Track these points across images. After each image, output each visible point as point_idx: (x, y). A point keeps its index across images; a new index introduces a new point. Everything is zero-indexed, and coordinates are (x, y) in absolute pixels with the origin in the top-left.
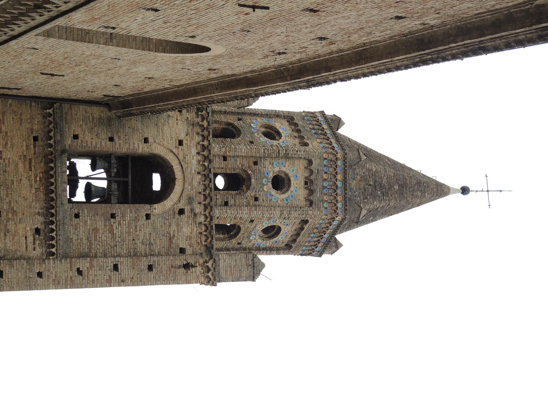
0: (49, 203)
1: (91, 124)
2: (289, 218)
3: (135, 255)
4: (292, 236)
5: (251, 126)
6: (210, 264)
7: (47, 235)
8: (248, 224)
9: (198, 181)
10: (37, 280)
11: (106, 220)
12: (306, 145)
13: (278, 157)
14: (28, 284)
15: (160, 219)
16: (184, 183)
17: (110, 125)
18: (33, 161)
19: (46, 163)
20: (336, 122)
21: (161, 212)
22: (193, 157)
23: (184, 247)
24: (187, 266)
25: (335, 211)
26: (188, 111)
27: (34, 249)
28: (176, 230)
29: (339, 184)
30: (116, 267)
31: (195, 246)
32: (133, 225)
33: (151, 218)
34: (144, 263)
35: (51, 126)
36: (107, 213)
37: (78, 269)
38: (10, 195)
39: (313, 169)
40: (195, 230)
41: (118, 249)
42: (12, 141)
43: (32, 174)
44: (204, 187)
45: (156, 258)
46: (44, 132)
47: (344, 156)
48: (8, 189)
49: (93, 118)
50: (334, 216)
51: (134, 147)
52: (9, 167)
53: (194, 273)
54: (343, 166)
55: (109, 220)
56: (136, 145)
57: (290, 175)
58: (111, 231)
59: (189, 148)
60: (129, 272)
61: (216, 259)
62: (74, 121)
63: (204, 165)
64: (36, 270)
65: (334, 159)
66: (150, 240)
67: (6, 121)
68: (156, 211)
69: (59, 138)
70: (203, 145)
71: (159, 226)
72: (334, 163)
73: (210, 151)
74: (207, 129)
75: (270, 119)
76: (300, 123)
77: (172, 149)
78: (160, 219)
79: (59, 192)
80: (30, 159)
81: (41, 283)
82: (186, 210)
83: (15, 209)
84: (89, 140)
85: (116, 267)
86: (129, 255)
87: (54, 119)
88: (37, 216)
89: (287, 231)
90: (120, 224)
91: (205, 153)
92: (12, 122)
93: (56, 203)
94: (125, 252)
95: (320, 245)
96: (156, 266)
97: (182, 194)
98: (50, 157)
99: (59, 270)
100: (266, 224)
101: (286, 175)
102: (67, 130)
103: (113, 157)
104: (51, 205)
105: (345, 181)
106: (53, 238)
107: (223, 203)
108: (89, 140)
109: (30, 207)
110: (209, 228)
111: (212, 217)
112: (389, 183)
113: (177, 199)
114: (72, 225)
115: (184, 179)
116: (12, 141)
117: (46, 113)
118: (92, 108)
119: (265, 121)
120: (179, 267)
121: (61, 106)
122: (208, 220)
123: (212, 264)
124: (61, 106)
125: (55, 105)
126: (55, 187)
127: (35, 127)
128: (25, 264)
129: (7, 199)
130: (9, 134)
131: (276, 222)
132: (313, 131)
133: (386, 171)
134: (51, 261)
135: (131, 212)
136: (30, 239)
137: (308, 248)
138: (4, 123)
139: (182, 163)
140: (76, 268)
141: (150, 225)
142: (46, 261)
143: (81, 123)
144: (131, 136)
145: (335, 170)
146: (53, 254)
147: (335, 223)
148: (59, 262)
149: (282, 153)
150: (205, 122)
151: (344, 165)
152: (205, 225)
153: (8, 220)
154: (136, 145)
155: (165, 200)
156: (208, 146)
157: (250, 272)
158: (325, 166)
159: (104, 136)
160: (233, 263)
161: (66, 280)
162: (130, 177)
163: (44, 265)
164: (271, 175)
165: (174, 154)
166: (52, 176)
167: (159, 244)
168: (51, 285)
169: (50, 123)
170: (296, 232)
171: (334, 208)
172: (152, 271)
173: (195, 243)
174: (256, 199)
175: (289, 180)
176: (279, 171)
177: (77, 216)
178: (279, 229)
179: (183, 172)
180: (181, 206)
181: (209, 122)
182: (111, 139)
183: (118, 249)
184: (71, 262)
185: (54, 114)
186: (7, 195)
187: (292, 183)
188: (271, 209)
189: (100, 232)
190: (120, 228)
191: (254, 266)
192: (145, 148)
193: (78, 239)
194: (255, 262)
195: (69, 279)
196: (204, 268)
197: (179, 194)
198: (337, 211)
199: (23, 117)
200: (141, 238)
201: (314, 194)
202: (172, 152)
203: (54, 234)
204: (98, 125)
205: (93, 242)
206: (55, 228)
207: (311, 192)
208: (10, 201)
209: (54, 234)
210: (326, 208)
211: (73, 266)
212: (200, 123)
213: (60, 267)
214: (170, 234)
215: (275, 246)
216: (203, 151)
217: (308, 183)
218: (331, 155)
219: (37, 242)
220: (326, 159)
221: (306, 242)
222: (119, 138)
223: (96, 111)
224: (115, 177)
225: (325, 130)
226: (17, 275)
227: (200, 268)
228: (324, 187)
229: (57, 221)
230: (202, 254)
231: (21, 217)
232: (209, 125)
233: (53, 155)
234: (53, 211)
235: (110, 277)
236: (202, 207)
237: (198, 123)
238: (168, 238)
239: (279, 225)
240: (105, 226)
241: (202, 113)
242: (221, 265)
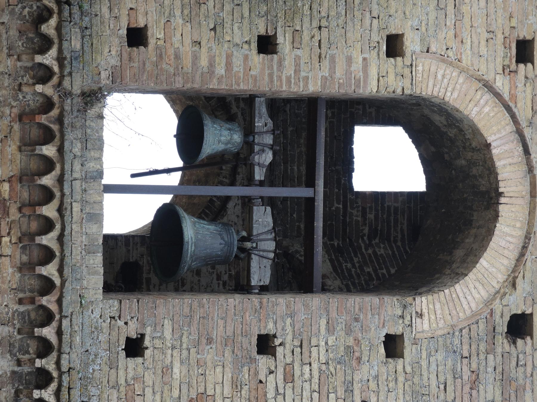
0: (32, 301)
11: (238, 365)
19: (28, 145)
32: (338, 381)
36: (245, 334)
46: (22, 17)
55: (252, 360)
56: (357, 66)
68: (423, 326)
69: (76, 44)
77: (489, 77)
78: (440, 356)
84: (187, 49)
90: (289, 378)
93: (59, 302)
97: (522, 255)
102: (105, 10)
103: (261, 111)
104: (42, 307)
113: (501, 278)
114: (116, 386)
126: (61, 239)
135: (330, 330)
141: (401, 379)
154: (357, 66)
162: (320, 183)
165: (497, 95)
166: (47, 196)
177: (134, 347)
182: (266, 45)
190: (289, 392)
192: (391, 77)
197: (513, 255)
202: (489, 87)
222: (295, 43)
224: (271, 180)
233: (55, 112)
240: (237, 385)
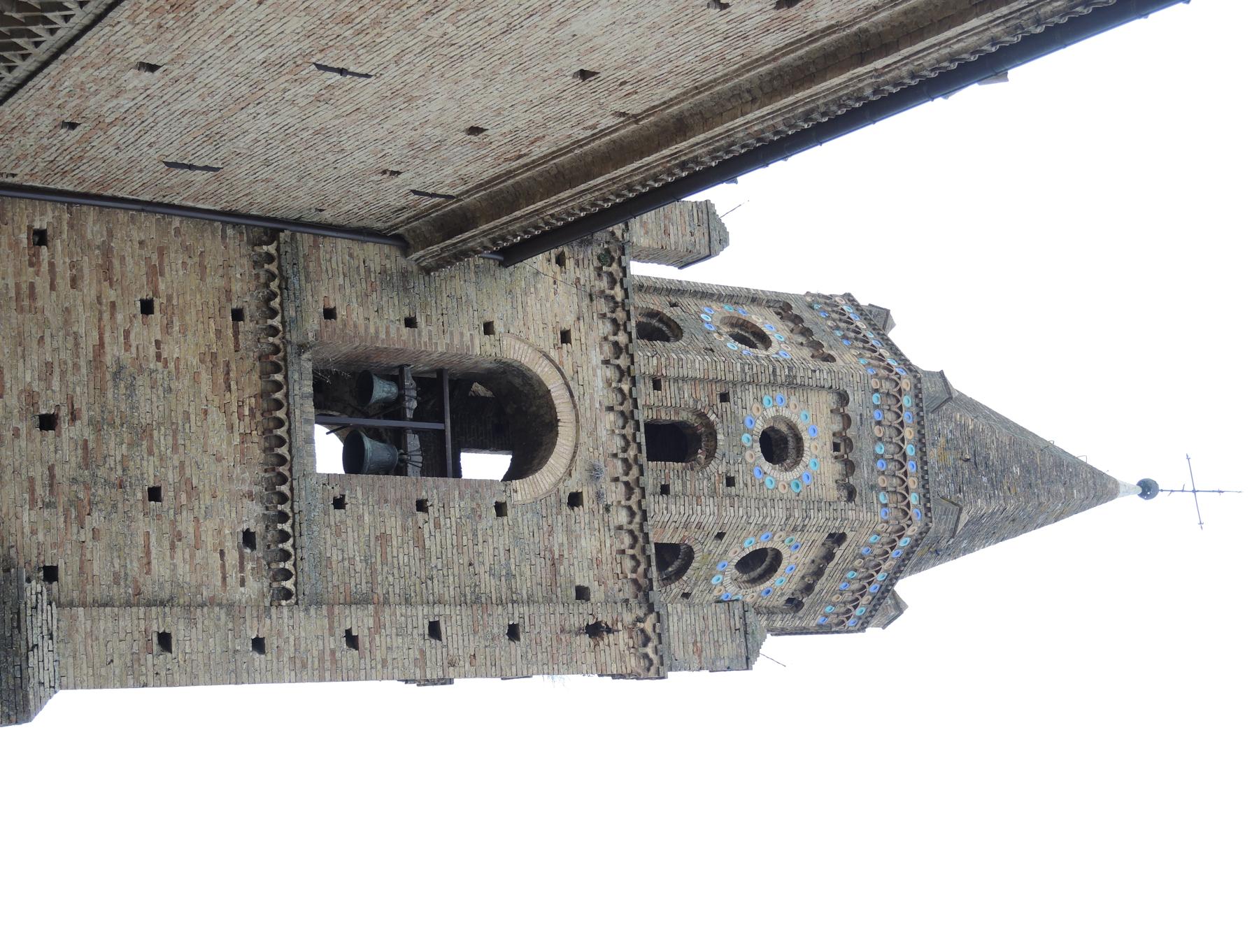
0: (273, 470)
1: (364, 285)
2: (804, 526)
3: (477, 600)
4: (803, 577)
5: (702, 321)
6: (648, 626)
7: (273, 547)
8: (711, 544)
9: (608, 427)
10: (255, 657)
11: (405, 517)
12: (829, 359)
13: (772, 384)
14: (232, 667)
15: (529, 515)
16: (577, 432)
17: (406, 290)
18: (233, 366)
19: (264, 374)
20: (879, 319)
21: (529, 499)
22: (594, 370)
23: (586, 584)
24: (595, 630)
25: (906, 514)
26: (577, 263)
27: (243, 583)
28: (565, 542)
29: (910, 450)
30: (434, 630)
31: (610, 583)
32: (468, 529)
33: (509, 513)
34: (499, 621)
35: (274, 285)
37: (348, 632)
38: (181, 449)
39: (850, 414)
40: (608, 545)
41: (437, 587)
42: (182, 318)
43: (233, 398)
44: (623, 444)
45: (526, 608)
47: (916, 386)
48: (175, 433)
49: (368, 270)
50: (904, 523)
51: (462, 341)
52: (178, 379)
53: (613, 647)
54: (914, 409)
55: (414, 514)
56: (467, 338)
57: (800, 427)
58: (419, 542)
59: (585, 350)
60: (466, 642)
61: (662, 612)
62: (324, 276)
63: (621, 390)
64: (249, 632)
65: (894, 391)
66: (508, 564)
67: (167, 269)
68: (518, 497)
69: (293, 313)
70: (616, 344)
71: (526, 532)
72: (894, 401)
73: (632, 356)
74: (623, 304)
75: (739, 308)
76: (806, 315)
77: (546, 350)
78: (529, 515)
79: (299, 440)
80: (227, 364)
81: (263, 666)
82: (585, 495)
83: (195, 482)
84: (361, 322)
85: (434, 630)
86: (462, 602)
87: (280, 267)
88: (246, 501)
89: (795, 564)
90: (437, 525)
91: (623, 361)
92: (181, 273)
94: (452, 593)
95: (864, 601)
96: (527, 629)
98: (274, 358)
99: (303, 634)
100: (750, 546)
101: (792, 427)
105: (921, 442)
106: (286, 556)
107: (659, 490)
108: (361, 322)
109: (230, 478)
110: (641, 540)
111: (644, 512)
112: (1003, 460)
113: (563, 470)
114: (329, 526)
115: (577, 421)
116: (182, 318)
117: (260, 255)
118: (365, 246)
119: (728, 309)
120: (578, 633)
121: (293, 237)
122: (637, 519)
123: (654, 626)
124: (293, 237)
125: (282, 235)
126: (289, 431)
127: (236, 287)
128: (223, 616)
129: (176, 457)
130: (175, 302)
131: (772, 539)
132: (839, 334)
133: (994, 432)
134: (285, 610)
135: (461, 497)
136: (232, 557)
137: (837, 610)
138: (162, 274)
139: (571, 384)
140: (343, 629)
142: (273, 610)
143: (341, 281)
144: (454, 317)
145: (899, 416)
146: (287, 594)
147: (903, 543)
148: (302, 614)
149: (782, 374)
150: (618, 288)
151: (917, 405)
152: (631, 532)
153: (179, 510)
154: (467, 338)
155: (536, 471)
156: (627, 346)
157: (739, 646)
158: (877, 407)
159: (394, 313)
160: (700, 625)
161: (321, 660)
163: (268, 621)
164: (760, 427)
165: (552, 361)
166: (279, 405)
167: (530, 577)
168: (286, 671)
169: (272, 276)
170: (813, 568)
171: (903, 505)
172: (519, 639)
173: (610, 575)
174: (730, 482)
175: (799, 440)
176: (775, 418)
178: (777, 557)
179: (575, 406)
180: (572, 486)
181: (626, 290)
182: (410, 323)
183: (437, 587)
184: (331, 615)
185: (279, 255)
186: (175, 448)
187: (806, 445)
188: (766, 506)
189: (394, 543)
190: (438, 535)
191: (746, 633)
192: (488, 346)
193: (343, 559)
194: (748, 621)
195: (327, 657)
196: (634, 634)
197: (570, 457)
198: (910, 513)
199: (208, 260)
200: (488, 559)
201: (857, 471)
202: (547, 356)
203: (288, 546)
204: (379, 289)
205: (379, 568)
206: (290, 530)
207: (850, 467)
208: (182, 464)
209: (288, 546)
210: (886, 505)
211: (336, 624)
212: (608, 292)
213: (298, 627)
214: (552, 552)
215: (764, 603)
216: (618, 358)
217: (842, 445)
218: (888, 383)
219: (249, 566)
220: (877, 391)
221: (834, 593)
223: (375, 255)
225: (864, 332)
226: (206, 644)
227: (626, 636)
228: (878, 457)
229: (294, 514)
230: (627, 601)
231: (208, 503)
232: (627, 296)
233: (281, 354)
234: (284, 489)
235: (423, 652)
236: (621, 488)
237: (603, 292)
238: (549, 563)
239: (779, 547)
240: (405, 529)
241: (610, 269)
242: (673, 628)
